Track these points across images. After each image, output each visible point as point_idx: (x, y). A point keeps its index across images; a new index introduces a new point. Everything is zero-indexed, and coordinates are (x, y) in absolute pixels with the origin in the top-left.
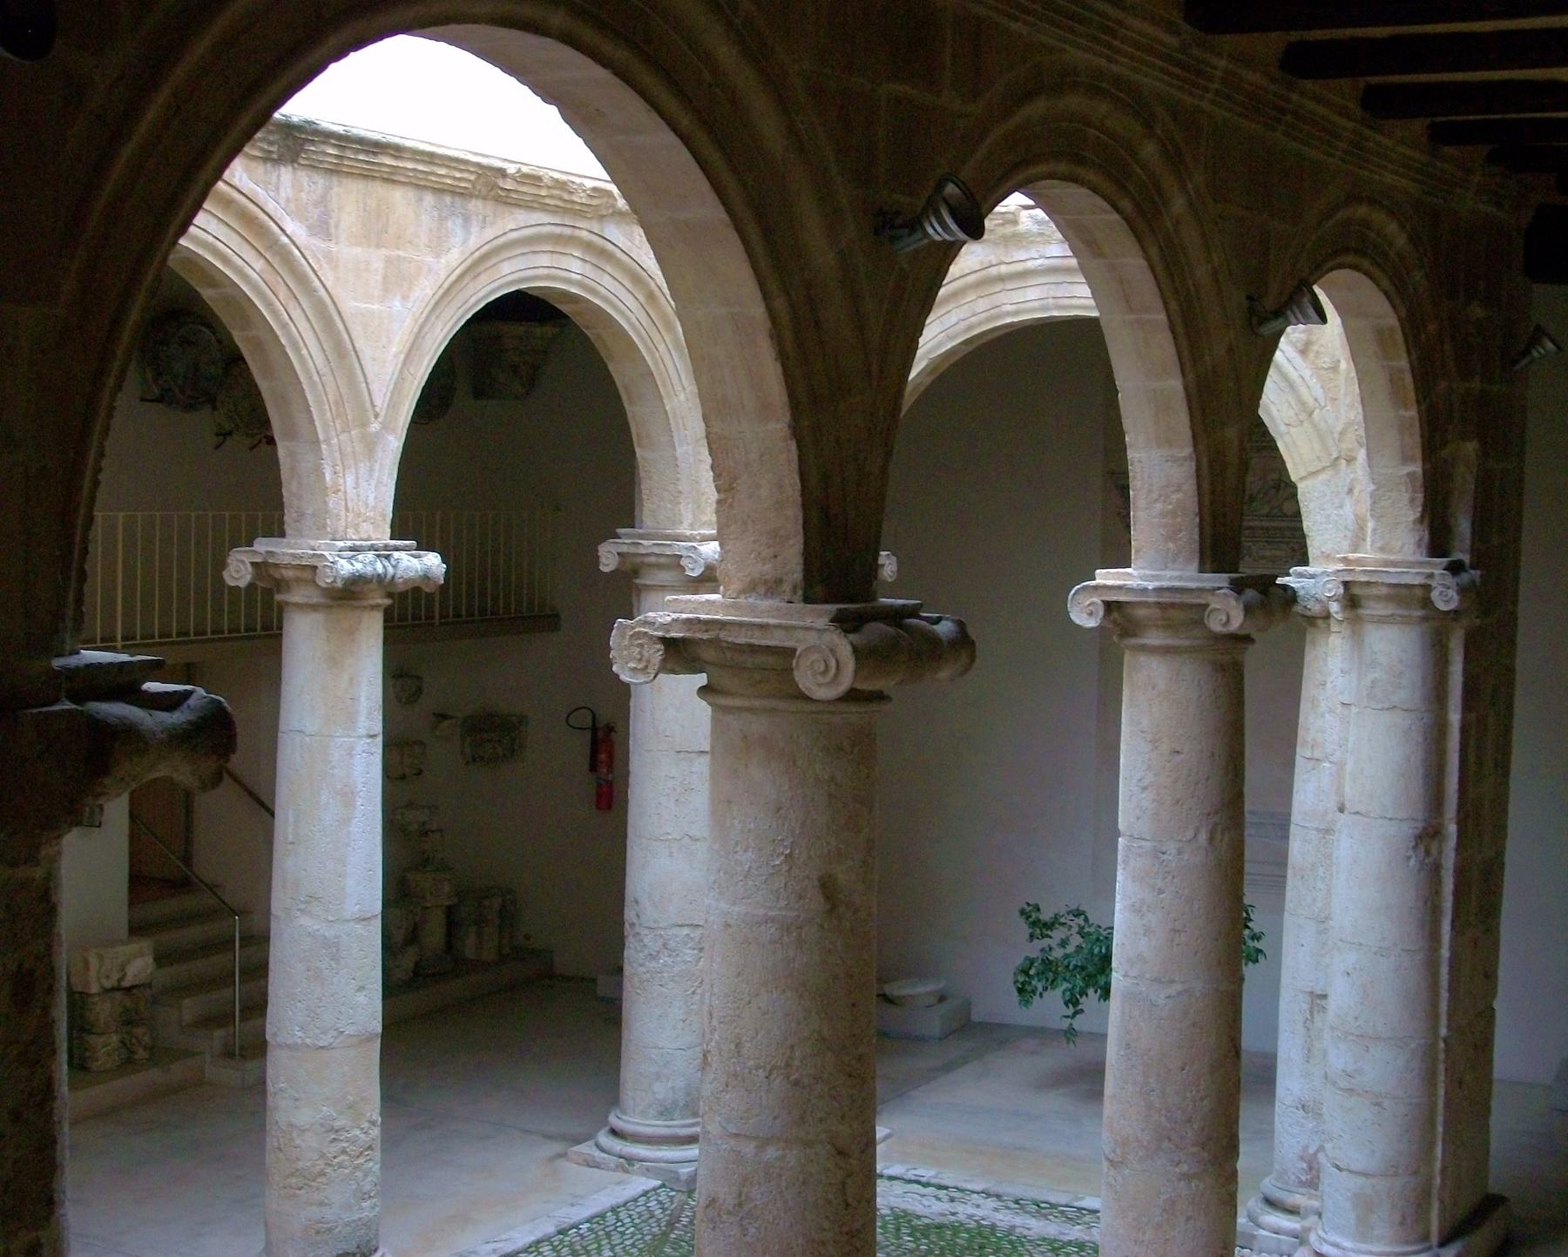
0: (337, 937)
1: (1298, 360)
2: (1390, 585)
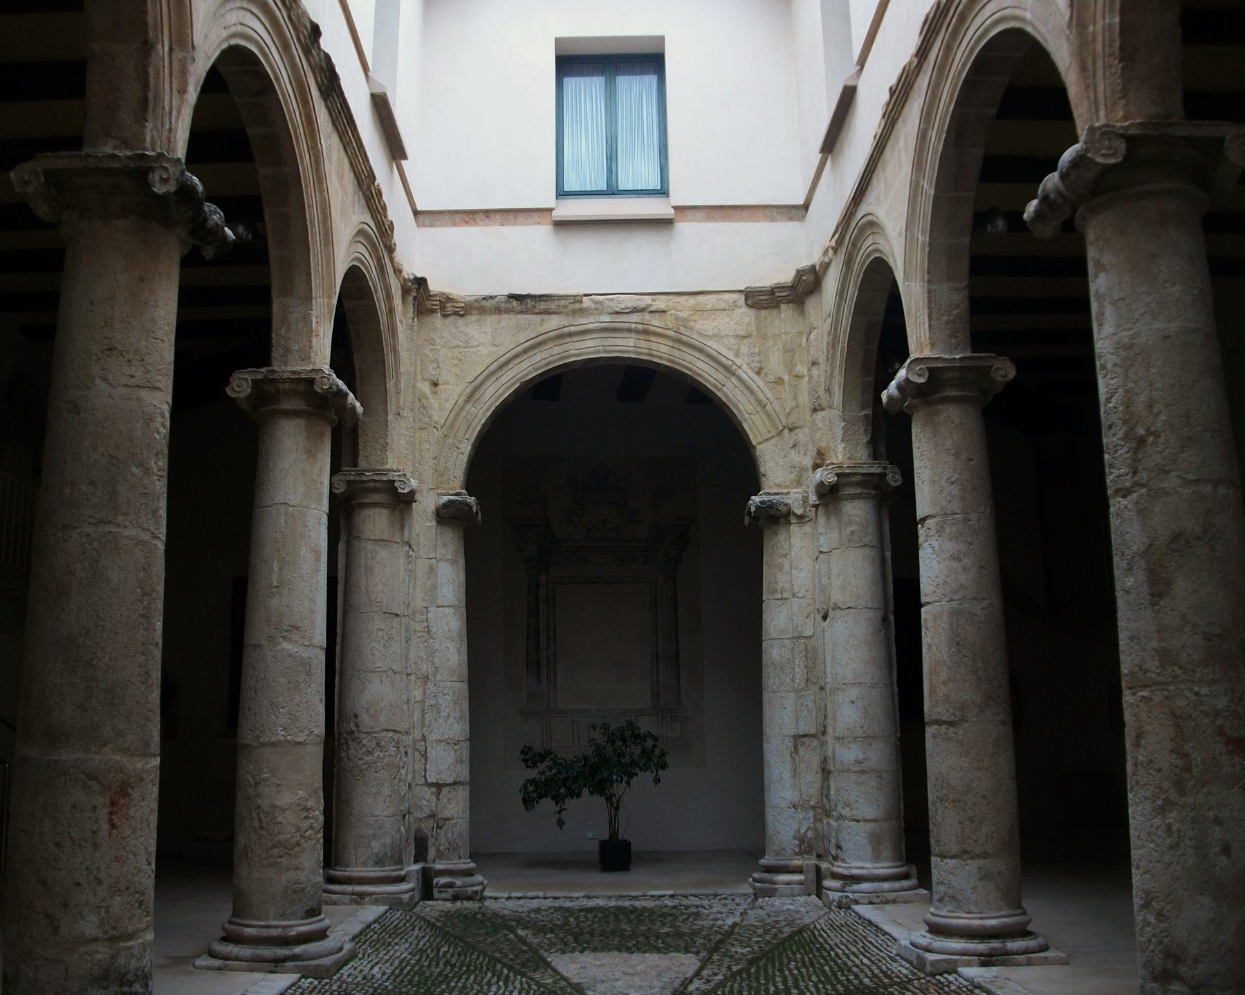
0: (310, 658)
1: (756, 378)
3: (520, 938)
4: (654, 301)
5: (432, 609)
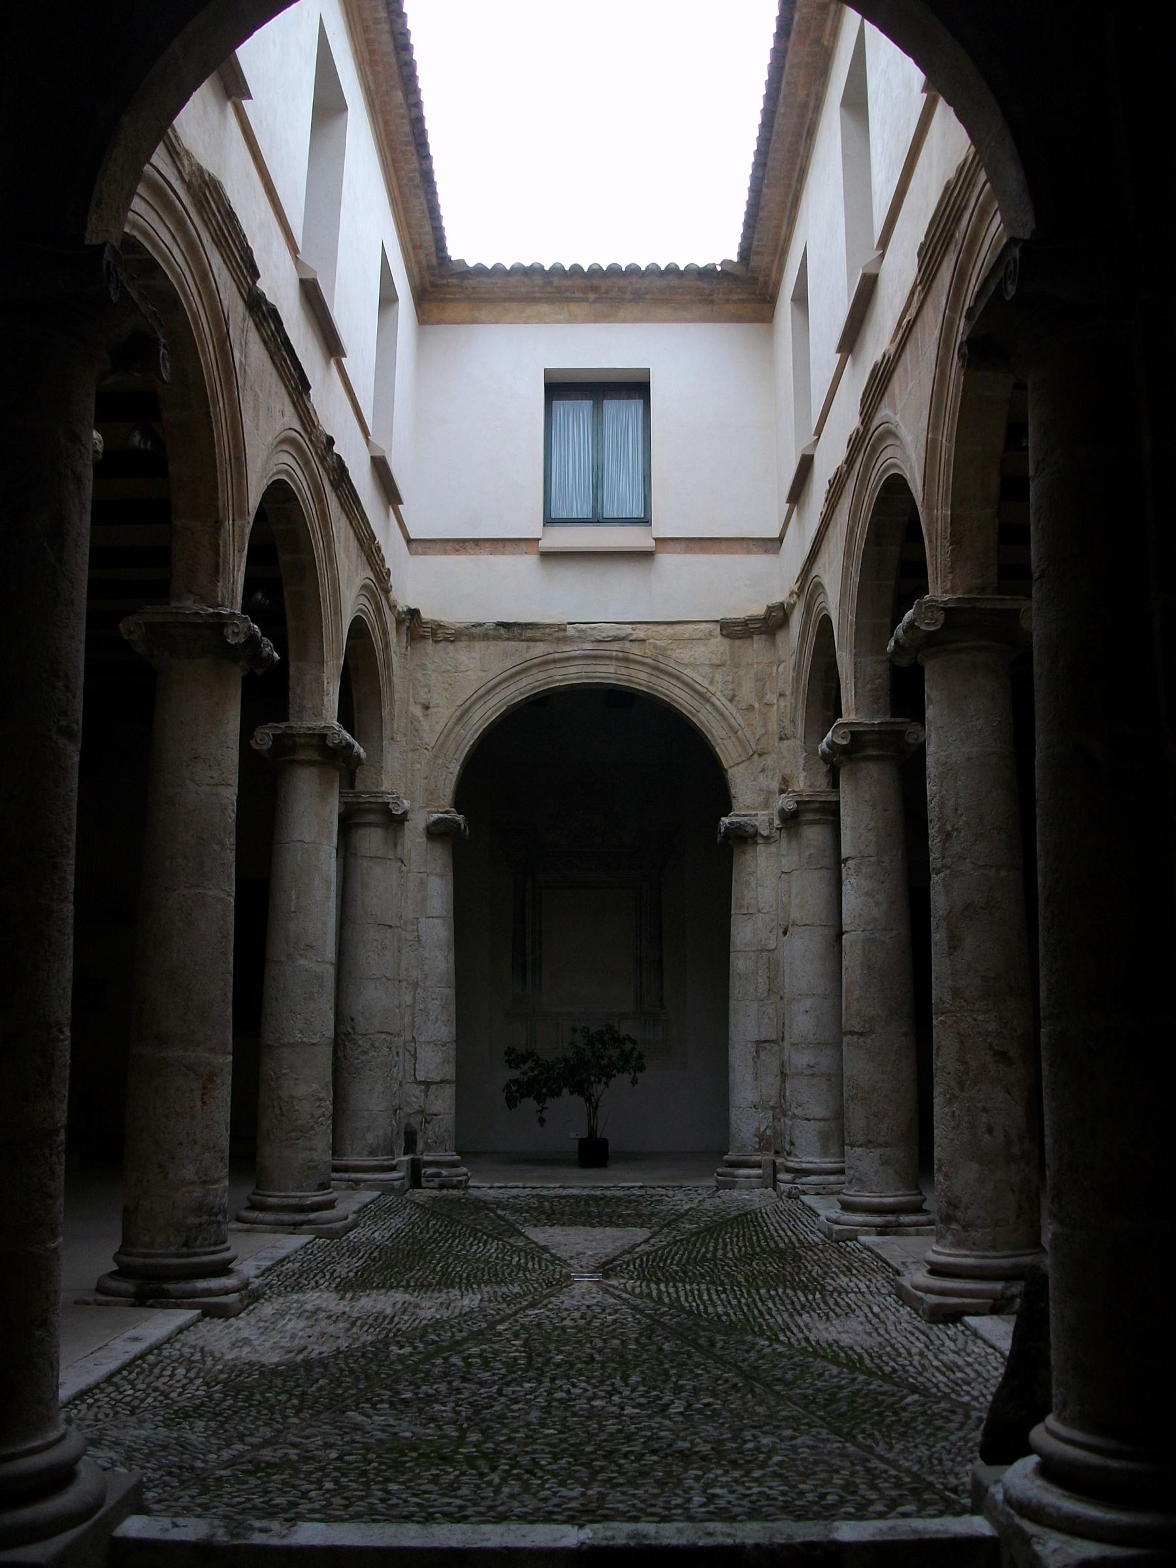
2: (820, 802)
3: (499, 1217)
4: (634, 630)
5: (422, 920)
